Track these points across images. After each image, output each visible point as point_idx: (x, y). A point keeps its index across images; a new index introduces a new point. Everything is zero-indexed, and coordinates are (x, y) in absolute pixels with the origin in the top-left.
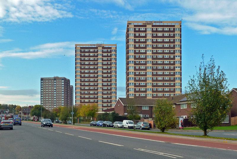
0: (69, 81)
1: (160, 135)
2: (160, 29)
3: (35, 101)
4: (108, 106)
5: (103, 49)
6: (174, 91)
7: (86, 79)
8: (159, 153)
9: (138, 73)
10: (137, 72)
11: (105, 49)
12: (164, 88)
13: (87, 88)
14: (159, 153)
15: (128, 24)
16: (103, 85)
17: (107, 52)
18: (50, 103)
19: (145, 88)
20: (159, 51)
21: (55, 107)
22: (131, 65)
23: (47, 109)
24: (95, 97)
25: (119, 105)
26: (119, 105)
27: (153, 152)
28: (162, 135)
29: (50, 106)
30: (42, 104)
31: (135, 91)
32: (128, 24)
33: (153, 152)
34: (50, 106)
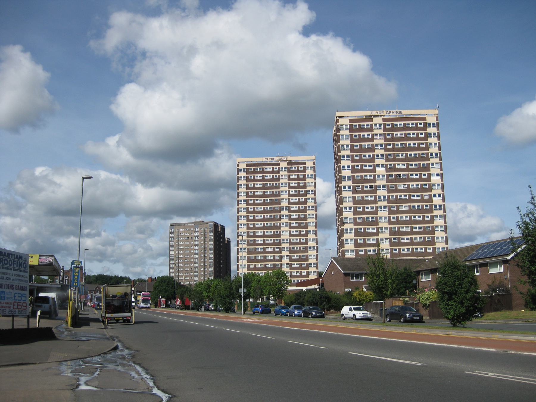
0: (223, 228)
1: (505, 337)
2: (399, 124)
3: (160, 269)
4: (301, 276)
5: (290, 166)
6: (433, 242)
7: (259, 224)
8: (488, 374)
9: (252, 234)
10: (252, 232)
11: (293, 166)
12: (413, 236)
13: (260, 240)
14: (488, 374)
15: (338, 118)
16: (290, 235)
17: (298, 171)
18: (186, 272)
19: (376, 237)
20: (366, 176)
21: (196, 279)
22: (347, 194)
23: (182, 283)
24: (276, 258)
25: (333, 273)
26: (333, 273)
27: (516, 379)
28: (501, 336)
29: (186, 278)
30: (172, 275)
31: (357, 245)
32: (338, 118)
33: (516, 379)
34: (186, 278)
